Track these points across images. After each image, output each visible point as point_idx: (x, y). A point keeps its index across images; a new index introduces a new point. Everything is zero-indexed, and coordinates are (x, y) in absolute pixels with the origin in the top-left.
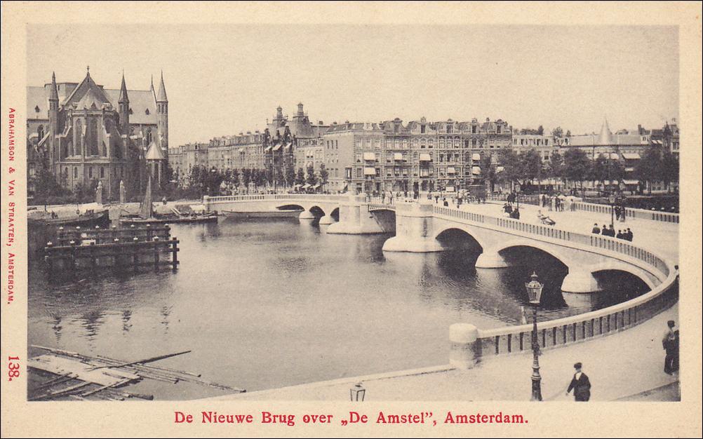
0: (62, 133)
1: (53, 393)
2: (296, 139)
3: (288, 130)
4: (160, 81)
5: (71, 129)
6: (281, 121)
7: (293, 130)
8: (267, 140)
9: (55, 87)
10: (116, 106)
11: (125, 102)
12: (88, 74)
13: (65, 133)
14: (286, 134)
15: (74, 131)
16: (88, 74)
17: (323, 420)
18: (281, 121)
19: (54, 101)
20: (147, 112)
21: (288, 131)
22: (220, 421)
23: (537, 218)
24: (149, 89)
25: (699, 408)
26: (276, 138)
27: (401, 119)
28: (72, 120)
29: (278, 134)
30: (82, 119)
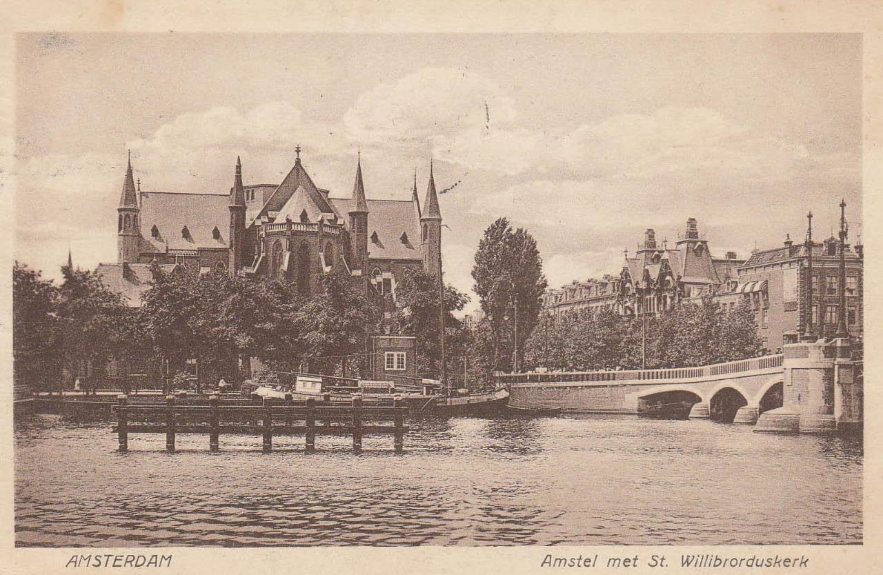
0: (248, 265)
1: (58, 417)
2: (682, 285)
3: (667, 266)
4: (357, 166)
5: (265, 259)
6: (651, 250)
7: (678, 269)
8: (624, 291)
9: (241, 192)
10: (344, 220)
11: (360, 218)
12: (298, 162)
13: (254, 268)
14: (662, 276)
15: (271, 259)
16: (298, 162)
17: (787, 564)
18: (651, 250)
19: (238, 211)
20: (404, 239)
21: (666, 270)
22: (785, 565)
23: (39, 269)
24: (409, 196)
25: (845, 551)
26: (643, 285)
27: (697, 219)
28: (266, 242)
29: (647, 277)
30: (284, 242)
